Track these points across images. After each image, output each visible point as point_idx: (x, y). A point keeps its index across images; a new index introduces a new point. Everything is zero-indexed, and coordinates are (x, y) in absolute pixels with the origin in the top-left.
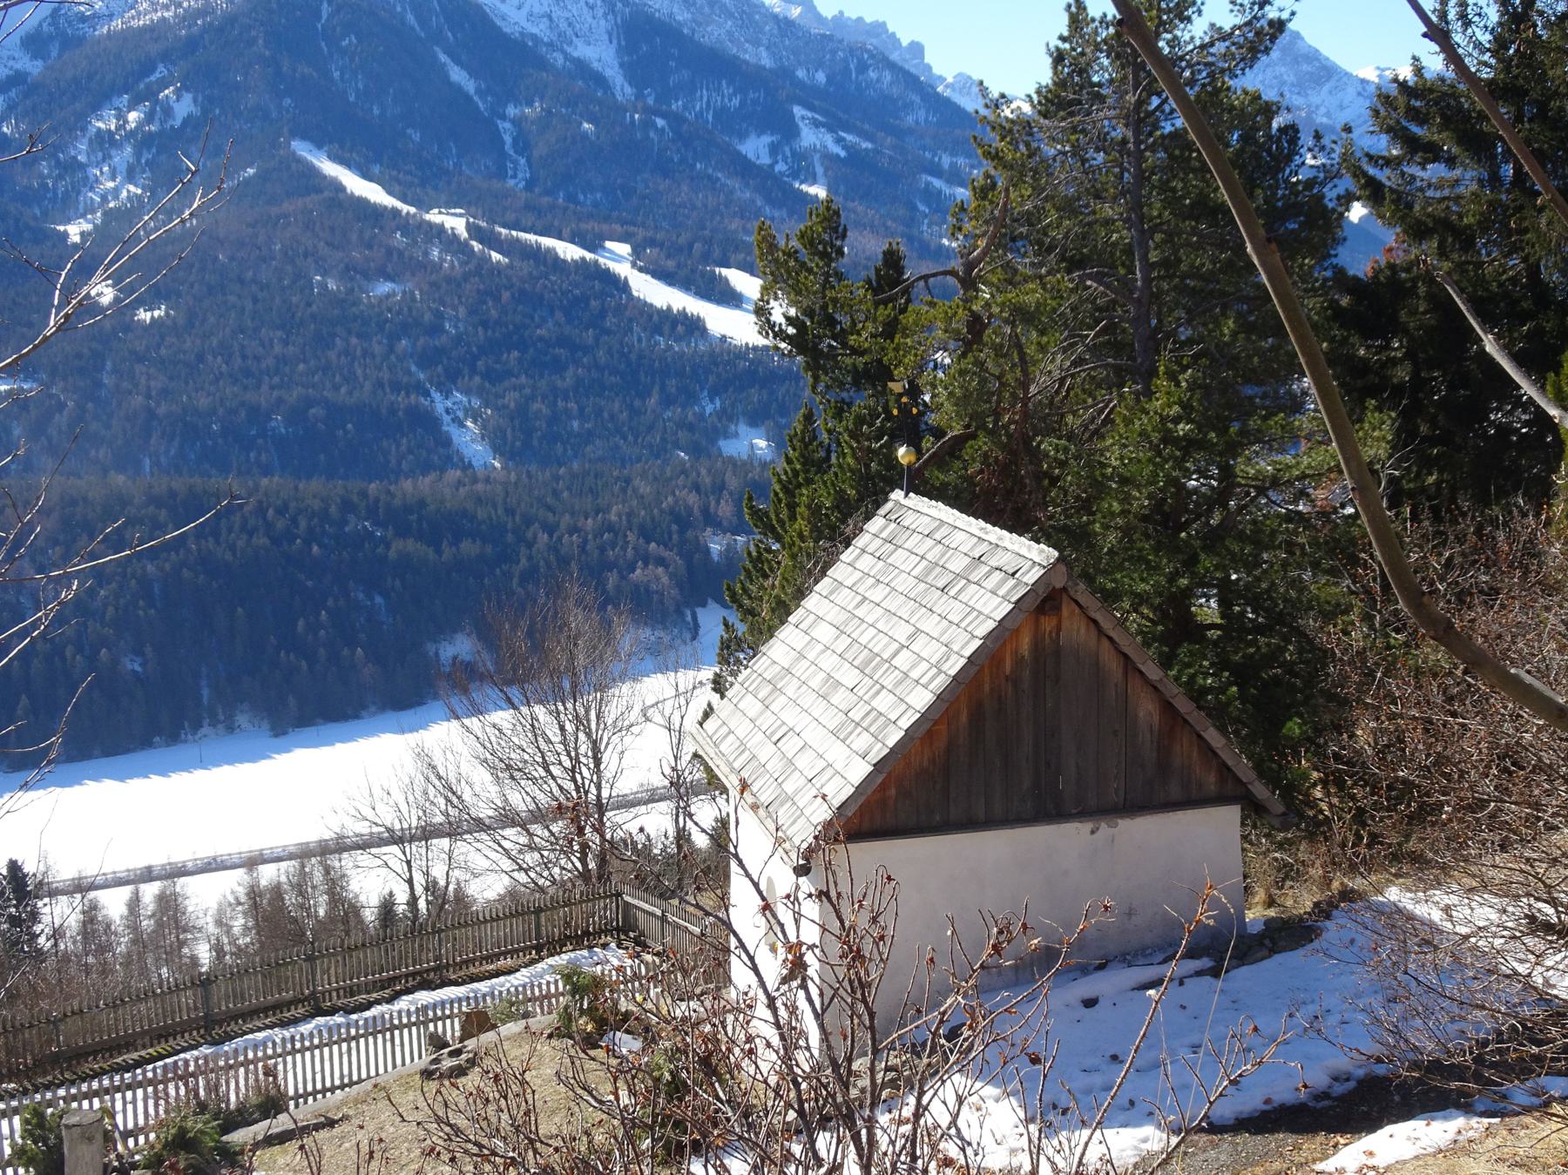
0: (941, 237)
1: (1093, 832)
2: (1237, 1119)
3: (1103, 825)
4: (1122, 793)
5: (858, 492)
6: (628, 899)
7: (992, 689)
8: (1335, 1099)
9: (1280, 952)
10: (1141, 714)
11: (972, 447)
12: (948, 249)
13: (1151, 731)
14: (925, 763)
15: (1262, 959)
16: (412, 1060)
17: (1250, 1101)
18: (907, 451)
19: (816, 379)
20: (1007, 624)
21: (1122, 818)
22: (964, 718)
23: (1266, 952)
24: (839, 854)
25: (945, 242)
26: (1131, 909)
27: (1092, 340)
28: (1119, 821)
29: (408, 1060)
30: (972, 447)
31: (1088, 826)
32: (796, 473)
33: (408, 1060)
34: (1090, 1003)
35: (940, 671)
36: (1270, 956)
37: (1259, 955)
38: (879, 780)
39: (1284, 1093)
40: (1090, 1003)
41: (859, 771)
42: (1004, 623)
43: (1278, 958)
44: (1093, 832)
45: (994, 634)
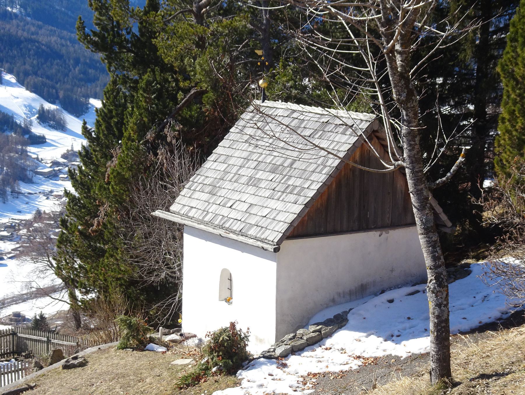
0: (6, 6)
1: (380, 236)
2: (471, 329)
3: (384, 233)
4: (390, 220)
5: (149, 120)
6: (19, 335)
7: (345, 174)
8: (505, 319)
9: (457, 280)
10: (398, 186)
11: (207, 97)
12: (11, 13)
13: (402, 193)
14: (319, 206)
15: (452, 282)
16: (5, 385)
17: (474, 323)
18: (264, 82)
19: (110, 64)
20: (356, 145)
21: (391, 229)
22: (334, 186)
23: (453, 279)
24: (287, 244)
25: (9, 9)
26: (392, 269)
27: (241, 49)
28: (390, 231)
29: (6, 384)
30: (207, 97)
31: (378, 233)
32: (110, 111)
33: (6, 384)
34: (391, 301)
35: (325, 166)
36: (455, 281)
37: (451, 281)
38: (307, 211)
39: (485, 320)
40: (391, 301)
41: (298, 209)
42: (355, 144)
43: (458, 282)
44: (380, 236)
45: (351, 149)
